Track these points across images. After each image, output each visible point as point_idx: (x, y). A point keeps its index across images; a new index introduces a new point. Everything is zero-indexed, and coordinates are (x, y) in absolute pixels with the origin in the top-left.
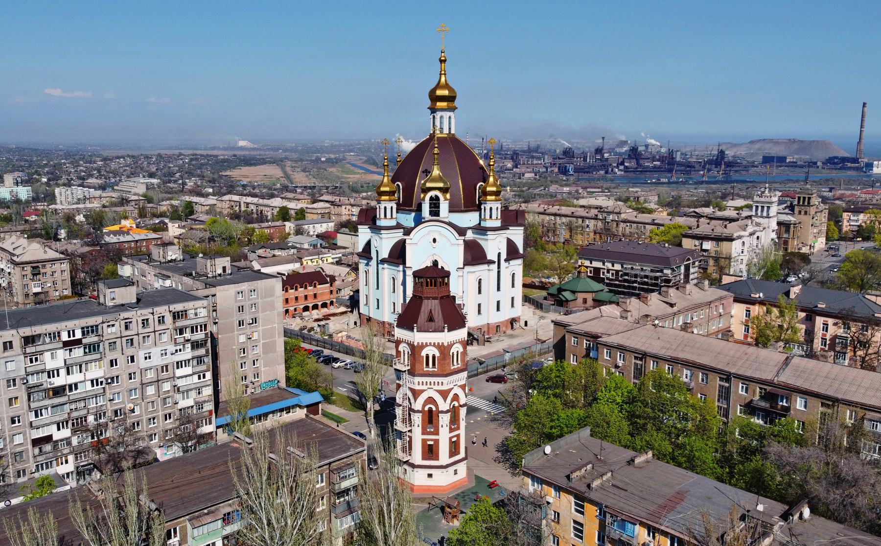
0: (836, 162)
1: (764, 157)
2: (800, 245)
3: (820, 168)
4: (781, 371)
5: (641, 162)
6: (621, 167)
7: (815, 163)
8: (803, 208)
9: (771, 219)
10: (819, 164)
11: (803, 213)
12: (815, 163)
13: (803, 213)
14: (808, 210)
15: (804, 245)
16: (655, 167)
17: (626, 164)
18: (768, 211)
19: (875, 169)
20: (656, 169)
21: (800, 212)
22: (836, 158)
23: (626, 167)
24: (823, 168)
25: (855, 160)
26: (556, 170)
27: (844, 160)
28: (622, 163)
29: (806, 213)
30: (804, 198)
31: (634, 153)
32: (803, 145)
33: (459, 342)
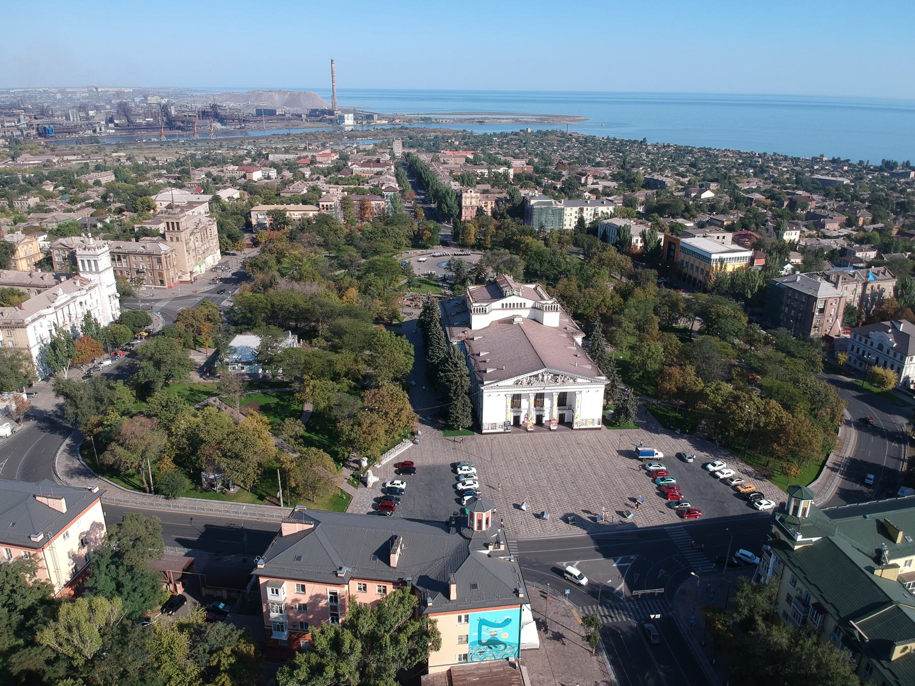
0: (316, 115)
1: (257, 110)
2: (180, 274)
3: (304, 120)
4: (855, 393)
5: (132, 118)
6: (111, 125)
7: (300, 116)
8: (173, 234)
9: (102, 275)
10: (304, 116)
11: (175, 239)
12: (300, 116)
13: (175, 239)
14: (179, 236)
15: (184, 273)
16: (148, 124)
17: (116, 122)
18: (96, 265)
19: (346, 121)
20: (149, 127)
21: (172, 239)
22: (317, 110)
23: (116, 125)
24: (307, 121)
25: (331, 113)
26: (34, 132)
27: (323, 112)
28: (111, 120)
29: (177, 239)
30: (173, 223)
31: (124, 110)
32: (294, 98)
33: (572, 429)
